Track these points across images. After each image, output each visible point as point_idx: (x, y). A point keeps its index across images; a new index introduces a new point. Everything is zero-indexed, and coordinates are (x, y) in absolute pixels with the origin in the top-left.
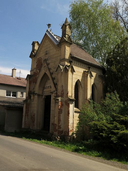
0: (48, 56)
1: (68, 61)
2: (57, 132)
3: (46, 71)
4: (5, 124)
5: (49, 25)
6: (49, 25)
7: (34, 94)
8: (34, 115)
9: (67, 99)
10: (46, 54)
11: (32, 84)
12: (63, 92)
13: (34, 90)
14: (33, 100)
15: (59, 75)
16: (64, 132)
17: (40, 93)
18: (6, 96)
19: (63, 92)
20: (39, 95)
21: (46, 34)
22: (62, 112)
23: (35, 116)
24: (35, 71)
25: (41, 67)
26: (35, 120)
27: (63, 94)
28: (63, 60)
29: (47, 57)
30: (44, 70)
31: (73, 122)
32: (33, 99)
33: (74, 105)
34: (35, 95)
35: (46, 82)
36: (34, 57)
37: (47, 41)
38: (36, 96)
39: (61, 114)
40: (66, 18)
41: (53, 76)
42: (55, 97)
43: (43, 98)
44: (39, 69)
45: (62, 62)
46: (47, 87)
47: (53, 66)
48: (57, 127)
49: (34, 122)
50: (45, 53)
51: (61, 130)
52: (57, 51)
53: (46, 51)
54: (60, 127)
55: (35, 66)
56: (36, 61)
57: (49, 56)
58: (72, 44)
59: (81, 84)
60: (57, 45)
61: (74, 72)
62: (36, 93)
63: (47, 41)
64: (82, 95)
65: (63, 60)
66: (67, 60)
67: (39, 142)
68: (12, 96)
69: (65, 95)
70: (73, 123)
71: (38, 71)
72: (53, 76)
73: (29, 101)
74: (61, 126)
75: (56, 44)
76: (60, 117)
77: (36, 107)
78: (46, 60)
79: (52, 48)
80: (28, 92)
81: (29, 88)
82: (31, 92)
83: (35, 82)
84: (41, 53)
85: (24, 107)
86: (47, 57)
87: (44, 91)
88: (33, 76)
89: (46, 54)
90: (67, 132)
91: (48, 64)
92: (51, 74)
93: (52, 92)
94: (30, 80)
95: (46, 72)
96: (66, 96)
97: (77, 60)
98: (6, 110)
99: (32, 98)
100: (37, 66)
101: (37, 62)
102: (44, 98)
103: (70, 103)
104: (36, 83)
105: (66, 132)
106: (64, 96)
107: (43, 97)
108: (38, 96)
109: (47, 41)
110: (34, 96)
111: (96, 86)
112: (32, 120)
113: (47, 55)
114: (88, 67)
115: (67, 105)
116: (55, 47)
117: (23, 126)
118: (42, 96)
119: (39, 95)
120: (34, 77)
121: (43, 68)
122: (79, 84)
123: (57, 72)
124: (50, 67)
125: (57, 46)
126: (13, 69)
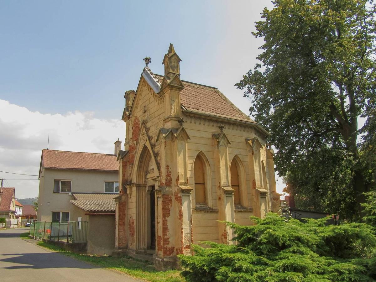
0: (147, 115)
1: (176, 120)
2: (162, 250)
3: (145, 142)
4: (88, 241)
5: (147, 60)
6: (147, 60)
7: (131, 184)
8: (133, 223)
9: (178, 189)
10: (145, 111)
11: (128, 167)
12: (170, 177)
13: (131, 178)
14: (130, 195)
15: (161, 147)
16: (175, 250)
17: (142, 182)
18: (105, 192)
19: (169, 178)
20: (138, 186)
21: (142, 76)
22: (169, 214)
23: (135, 224)
24: (130, 143)
25: (138, 135)
26: (135, 230)
27: (170, 181)
28: (167, 119)
29: (146, 117)
30: (143, 141)
31: (191, 231)
32: (131, 194)
33: (233, 200)
34: (132, 186)
35: (150, 161)
36: (129, 118)
37: (146, 87)
38: (134, 189)
39: (168, 217)
40: (171, 45)
41: (156, 150)
42: (159, 187)
43: (147, 191)
44: (136, 140)
45: (166, 123)
46: (151, 170)
47: (155, 131)
48: (162, 241)
49: (133, 234)
50: (143, 109)
51: (169, 246)
52: (159, 104)
53: (145, 107)
54: (166, 241)
55: (131, 136)
56: (132, 126)
57: (148, 115)
58: (182, 89)
59: (207, 160)
60: (158, 93)
61: (188, 139)
62: (134, 182)
63: (146, 87)
64: (210, 179)
65: (167, 119)
66: (174, 119)
67: (320, 278)
68: (115, 192)
69: (174, 182)
70: (192, 234)
71: (135, 142)
72: (156, 150)
73: (123, 198)
74: (169, 240)
75: (156, 92)
76: (167, 223)
77: (135, 207)
78: (144, 123)
79: (152, 99)
80: (122, 182)
81: (124, 175)
82: (126, 181)
83: (132, 163)
84: (138, 110)
85: (116, 211)
86: (146, 117)
87: (147, 177)
88: (128, 152)
89: (145, 111)
90: (181, 249)
91: (147, 130)
92: (153, 146)
93: (155, 179)
94: (125, 160)
95: (145, 144)
96: (176, 185)
97: (194, 117)
98: (88, 216)
99: (128, 192)
100: (133, 134)
101: (133, 128)
102: (148, 191)
103: (183, 196)
104: (132, 165)
105: (179, 249)
106: (173, 185)
107: (147, 189)
108: (137, 187)
109: (145, 88)
110: (131, 188)
111: (241, 160)
112: (131, 231)
113: (146, 113)
114: (220, 127)
115: (177, 200)
116: (156, 99)
117: (117, 244)
118: (145, 187)
119: (138, 186)
120: (130, 154)
121: (140, 137)
122: (205, 161)
123: (158, 142)
124: (150, 135)
125: (158, 95)
126: (117, 142)
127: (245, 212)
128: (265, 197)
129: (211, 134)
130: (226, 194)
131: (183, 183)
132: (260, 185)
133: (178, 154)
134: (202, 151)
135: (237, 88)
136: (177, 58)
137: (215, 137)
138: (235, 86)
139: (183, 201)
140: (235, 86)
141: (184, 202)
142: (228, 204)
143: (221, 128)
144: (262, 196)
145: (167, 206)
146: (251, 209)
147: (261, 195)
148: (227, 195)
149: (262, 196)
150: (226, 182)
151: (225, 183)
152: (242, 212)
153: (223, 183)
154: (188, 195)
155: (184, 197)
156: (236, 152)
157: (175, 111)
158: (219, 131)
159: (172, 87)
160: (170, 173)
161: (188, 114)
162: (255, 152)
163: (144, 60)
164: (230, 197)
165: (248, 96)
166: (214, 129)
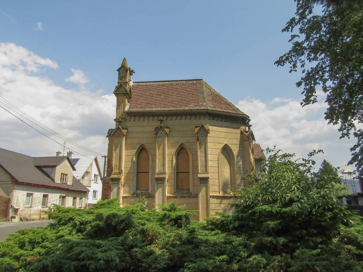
19: (109, 169)
127: (189, 197)
128: (207, 182)
129: (154, 128)
130: (157, 181)
131: (117, 173)
132: (205, 170)
133: (114, 149)
134: (144, 144)
135: (277, 66)
136: (125, 69)
137: (158, 130)
138: (275, 64)
139: (112, 188)
140: (275, 64)
141: (113, 189)
142: (160, 189)
143: (161, 121)
144: (201, 182)
145: (106, 192)
146: (195, 194)
147: (200, 181)
148: (158, 182)
149: (201, 182)
150: (162, 169)
151: (161, 170)
152: (185, 197)
153: (158, 171)
154: (117, 182)
155: (113, 185)
156: (182, 140)
157: (121, 114)
158: (158, 124)
159: (118, 94)
160: (111, 165)
161: (132, 114)
162: (200, 138)
163: (134, 72)
164: (162, 183)
165: (296, 71)
166: (155, 123)
